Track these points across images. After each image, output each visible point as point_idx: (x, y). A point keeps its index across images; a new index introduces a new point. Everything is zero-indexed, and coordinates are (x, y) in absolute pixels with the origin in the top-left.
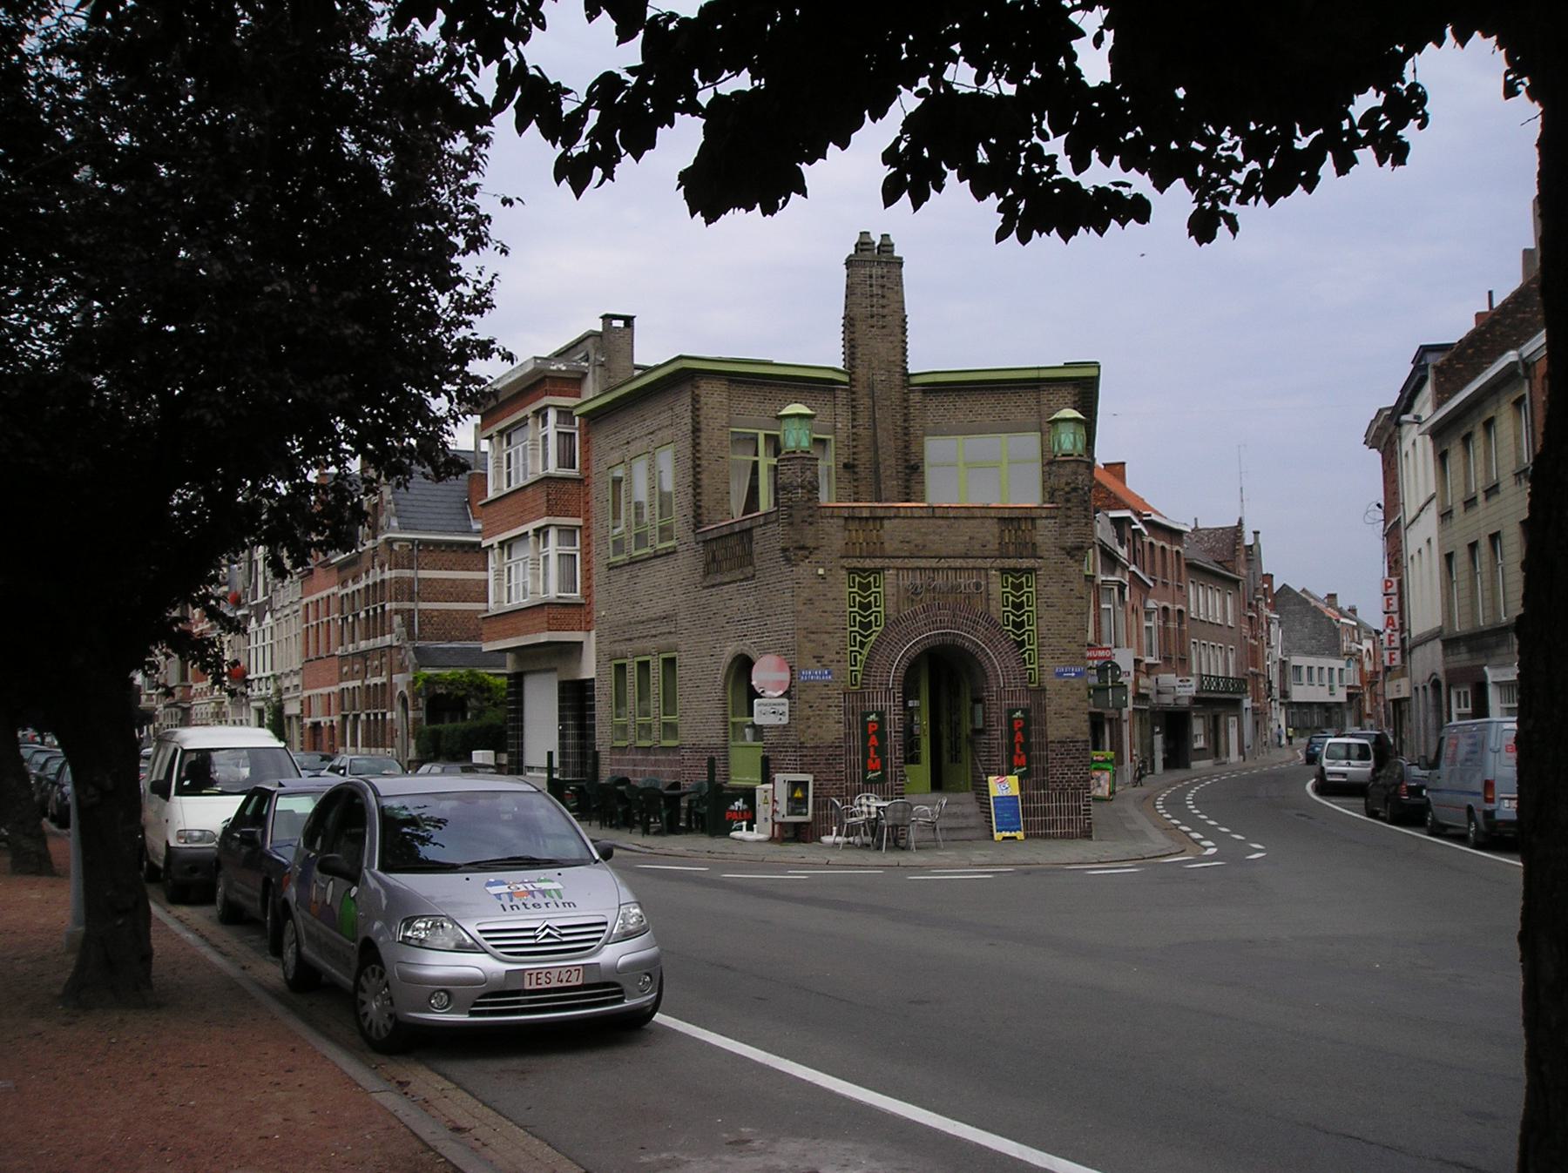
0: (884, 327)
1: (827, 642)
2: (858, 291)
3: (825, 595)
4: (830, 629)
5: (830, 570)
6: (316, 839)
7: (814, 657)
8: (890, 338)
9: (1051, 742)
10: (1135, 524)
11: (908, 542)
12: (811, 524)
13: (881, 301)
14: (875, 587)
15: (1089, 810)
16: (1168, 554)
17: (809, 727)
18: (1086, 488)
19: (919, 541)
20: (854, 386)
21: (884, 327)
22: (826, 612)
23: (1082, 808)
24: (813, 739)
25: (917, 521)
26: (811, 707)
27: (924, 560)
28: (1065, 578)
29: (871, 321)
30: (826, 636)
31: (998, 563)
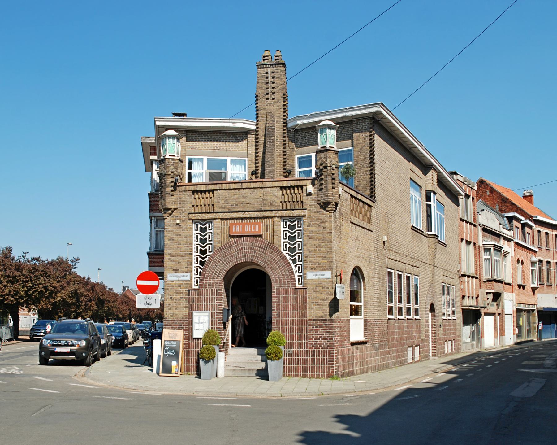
0: (273, 99)
1: (181, 261)
2: (260, 81)
3: (180, 235)
4: (182, 254)
5: (183, 221)
6: (250, 405)
7: (173, 270)
8: (278, 104)
9: (310, 320)
10: (523, 220)
11: (227, 203)
12: (172, 195)
13: (273, 85)
14: (209, 230)
15: (289, 354)
16: (550, 237)
17: (170, 309)
18: (334, 166)
19: (233, 202)
20: (258, 131)
21: (273, 99)
22: (181, 244)
23: (328, 360)
24: (172, 316)
25: (233, 191)
26: (171, 298)
27: (235, 213)
28: (320, 221)
29: (267, 96)
30: (180, 258)
31: (280, 213)
